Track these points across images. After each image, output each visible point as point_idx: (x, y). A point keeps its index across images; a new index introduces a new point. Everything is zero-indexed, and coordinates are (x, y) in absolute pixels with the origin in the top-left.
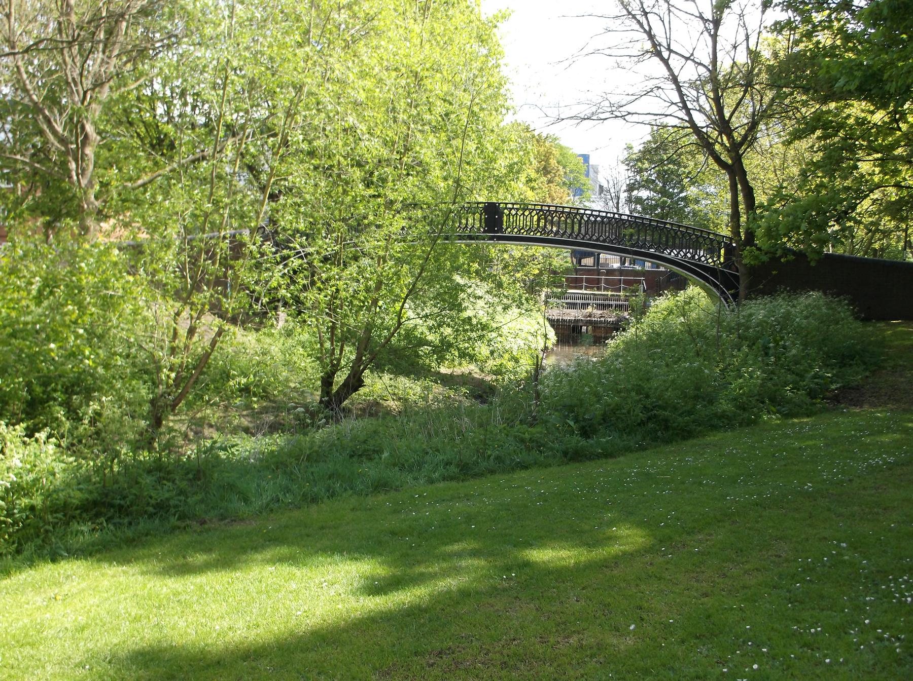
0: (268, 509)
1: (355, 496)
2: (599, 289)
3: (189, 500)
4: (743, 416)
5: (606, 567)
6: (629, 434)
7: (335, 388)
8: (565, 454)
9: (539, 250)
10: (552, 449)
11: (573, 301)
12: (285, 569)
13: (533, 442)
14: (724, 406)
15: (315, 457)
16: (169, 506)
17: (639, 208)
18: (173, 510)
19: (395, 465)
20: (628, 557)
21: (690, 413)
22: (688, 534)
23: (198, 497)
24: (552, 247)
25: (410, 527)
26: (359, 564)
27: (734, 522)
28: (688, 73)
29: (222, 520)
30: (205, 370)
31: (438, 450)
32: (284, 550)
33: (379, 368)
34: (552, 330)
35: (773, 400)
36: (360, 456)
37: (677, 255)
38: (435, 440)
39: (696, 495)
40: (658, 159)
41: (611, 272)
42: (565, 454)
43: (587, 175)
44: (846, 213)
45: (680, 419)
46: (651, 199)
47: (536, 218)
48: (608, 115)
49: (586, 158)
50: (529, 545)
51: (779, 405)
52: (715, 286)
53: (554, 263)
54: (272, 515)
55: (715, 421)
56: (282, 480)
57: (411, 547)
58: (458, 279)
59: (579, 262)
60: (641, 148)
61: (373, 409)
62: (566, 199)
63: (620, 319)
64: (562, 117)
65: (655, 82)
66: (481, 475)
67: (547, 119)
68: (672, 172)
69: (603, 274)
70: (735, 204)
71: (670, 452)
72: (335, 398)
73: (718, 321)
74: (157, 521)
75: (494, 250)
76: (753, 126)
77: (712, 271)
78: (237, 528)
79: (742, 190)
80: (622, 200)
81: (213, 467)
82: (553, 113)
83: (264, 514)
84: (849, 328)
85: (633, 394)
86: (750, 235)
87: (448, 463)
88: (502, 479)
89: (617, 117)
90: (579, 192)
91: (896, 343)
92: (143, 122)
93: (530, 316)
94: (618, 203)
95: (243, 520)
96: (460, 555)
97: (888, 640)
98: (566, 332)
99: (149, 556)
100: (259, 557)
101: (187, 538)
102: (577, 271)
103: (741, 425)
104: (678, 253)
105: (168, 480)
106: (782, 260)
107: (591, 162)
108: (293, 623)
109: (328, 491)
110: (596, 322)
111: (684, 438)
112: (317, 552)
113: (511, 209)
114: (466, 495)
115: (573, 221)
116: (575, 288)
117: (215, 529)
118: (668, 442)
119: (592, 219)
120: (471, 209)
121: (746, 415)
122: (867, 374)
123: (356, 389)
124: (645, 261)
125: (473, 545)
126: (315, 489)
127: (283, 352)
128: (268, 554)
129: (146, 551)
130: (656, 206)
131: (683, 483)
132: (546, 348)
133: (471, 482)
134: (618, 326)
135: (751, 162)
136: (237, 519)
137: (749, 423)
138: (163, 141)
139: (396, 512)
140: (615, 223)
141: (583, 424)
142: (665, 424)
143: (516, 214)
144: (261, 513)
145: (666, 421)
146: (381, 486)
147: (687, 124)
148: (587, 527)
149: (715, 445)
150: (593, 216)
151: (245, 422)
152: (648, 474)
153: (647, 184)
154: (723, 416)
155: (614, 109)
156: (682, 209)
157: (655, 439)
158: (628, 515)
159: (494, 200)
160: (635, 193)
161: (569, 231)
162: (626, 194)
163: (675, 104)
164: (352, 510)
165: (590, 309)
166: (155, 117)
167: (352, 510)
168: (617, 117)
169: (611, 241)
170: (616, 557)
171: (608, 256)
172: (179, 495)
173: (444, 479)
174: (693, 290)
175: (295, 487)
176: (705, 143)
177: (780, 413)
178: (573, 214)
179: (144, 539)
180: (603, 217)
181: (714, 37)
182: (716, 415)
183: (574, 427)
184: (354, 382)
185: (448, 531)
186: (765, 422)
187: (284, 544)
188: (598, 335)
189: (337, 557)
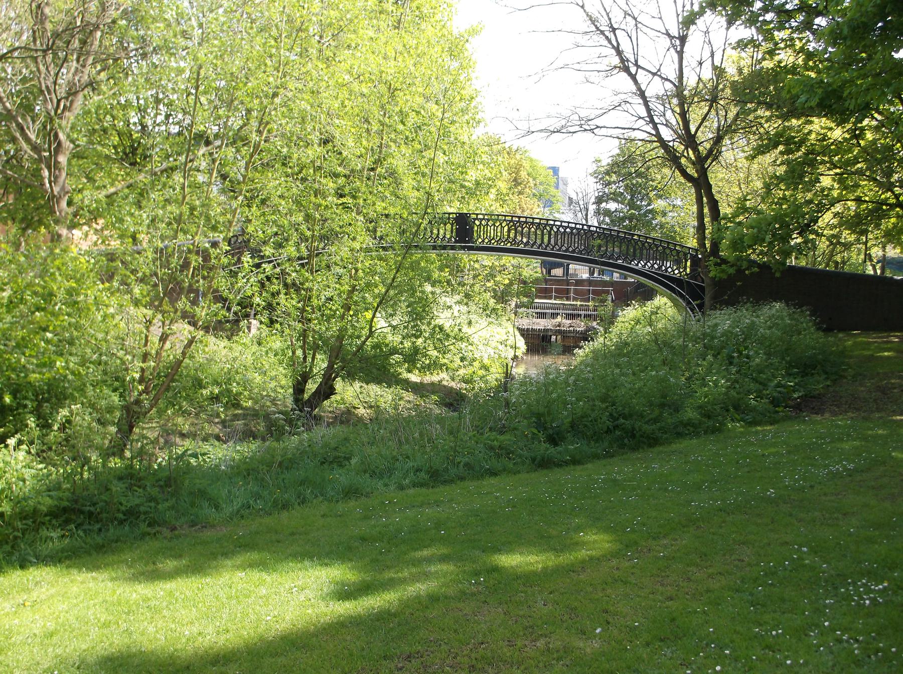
0: (238, 515)
2: (568, 299)
4: (709, 423)
7: (306, 396)
8: (534, 460)
9: (509, 260)
10: (520, 456)
12: (256, 575)
14: (690, 414)
15: (288, 464)
16: (140, 512)
18: (142, 517)
20: (594, 562)
21: (655, 421)
22: (654, 539)
23: (167, 504)
24: (522, 258)
28: (655, 88)
29: (193, 526)
31: (408, 457)
32: (255, 556)
33: (351, 376)
34: (522, 339)
35: (737, 408)
36: (331, 462)
40: (626, 172)
41: (580, 282)
42: (534, 460)
43: (557, 187)
44: (808, 225)
47: (506, 229)
48: (577, 128)
49: (555, 170)
50: (498, 550)
53: (524, 273)
55: (680, 429)
56: (252, 486)
57: (381, 553)
59: (549, 272)
60: (609, 161)
61: (347, 417)
62: (536, 210)
63: (589, 329)
64: (532, 129)
65: (623, 97)
66: (451, 481)
69: (572, 284)
70: (700, 216)
71: (638, 459)
72: (308, 401)
73: (684, 331)
74: (127, 528)
75: (465, 257)
76: (718, 140)
77: (678, 282)
78: (208, 534)
82: (524, 126)
83: (235, 520)
84: (810, 337)
86: (715, 245)
87: (418, 470)
88: (471, 485)
89: (586, 130)
90: (549, 203)
91: (856, 353)
94: (587, 215)
95: (213, 526)
96: (429, 560)
97: (847, 641)
98: (536, 342)
100: (229, 563)
101: (156, 544)
102: (546, 281)
105: (139, 487)
106: (747, 272)
107: (561, 174)
108: (262, 628)
109: (299, 497)
111: (651, 446)
112: (287, 558)
114: (436, 502)
115: (543, 232)
116: (545, 298)
118: (635, 449)
119: (562, 230)
120: (443, 220)
121: (711, 423)
122: (828, 383)
123: (327, 396)
125: (444, 551)
127: (256, 360)
128: (239, 560)
129: (115, 558)
131: (649, 489)
134: (586, 336)
135: (717, 176)
137: (714, 431)
138: (136, 149)
139: (366, 518)
140: (584, 234)
141: (551, 432)
143: (487, 225)
144: (231, 519)
146: (351, 492)
148: (554, 533)
149: (681, 453)
152: (615, 481)
153: (615, 197)
154: (689, 424)
155: (583, 122)
157: (622, 446)
158: (596, 520)
160: (604, 205)
161: (539, 242)
162: (594, 206)
163: (642, 118)
164: (323, 516)
165: (559, 319)
167: (323, 516)
168: (586, 130)
169: (580, 252)
170: (583, 561)
172: (150, 501)
174: (662, 301)
176: (673, 158)
177: (744, 421)
178: (543, 225)
179: (114, 545)
180: (572, 229)
181: (680, 54)
184: (326, 390)
185: (417, 537)
186: (729, 430)
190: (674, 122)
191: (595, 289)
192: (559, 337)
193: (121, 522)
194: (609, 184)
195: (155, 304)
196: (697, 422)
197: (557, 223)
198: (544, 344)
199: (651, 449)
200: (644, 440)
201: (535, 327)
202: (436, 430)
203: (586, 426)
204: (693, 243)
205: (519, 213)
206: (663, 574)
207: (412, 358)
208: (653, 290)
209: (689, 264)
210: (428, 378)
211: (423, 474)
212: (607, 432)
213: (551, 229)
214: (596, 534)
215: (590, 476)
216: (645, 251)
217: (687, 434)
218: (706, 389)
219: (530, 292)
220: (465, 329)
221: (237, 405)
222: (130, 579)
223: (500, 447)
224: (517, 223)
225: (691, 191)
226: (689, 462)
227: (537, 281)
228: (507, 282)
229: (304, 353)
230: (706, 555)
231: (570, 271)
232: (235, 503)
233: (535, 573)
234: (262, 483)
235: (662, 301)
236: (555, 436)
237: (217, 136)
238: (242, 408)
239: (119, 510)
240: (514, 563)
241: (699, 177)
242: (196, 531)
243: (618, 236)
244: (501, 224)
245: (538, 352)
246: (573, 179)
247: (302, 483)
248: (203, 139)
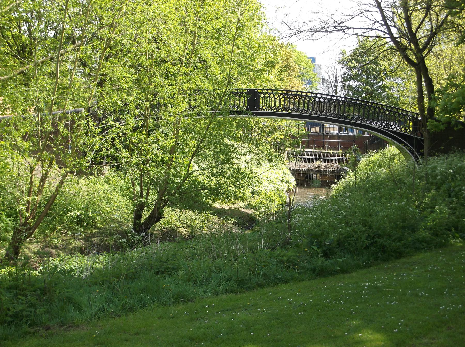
0: (96, 317)
1: (161, 306)
2: (324, 148)
3: (38, 311)
7: (143, 220)
8: (314, 270)
9: (284, 122)
10: (303, 268)
11: (307, 157)
16: (23, 316)
17: (350, 93)
18: (25, 319)
19: (189, 281)
21: (400, 239)
22: (417, 338)
23: (43, 309)
24: (292, 120)
27: (449, 328)
29: (62, 326)
30: (52, 206)
31: (220, 269)
33: (173, 205)
34: (293, 177)
36: (163, 273)
37: (375, 125)
39: (416, 305)
40: (363, 62)
41: (332, 137)
42: (314, 270)
43: (314, 71)
45: (394, 244)
46: (359, 87)
47: (283, 99)
48: (332, 29)
49: (313, 59)
51: (461, 232)
52: (405, 145)
53: (294, 131)
54: (100, 322)
56: (107, 294)
58: (227, 141)
59: (309, 130)
60: (351, 53)
61: (171, 235)
62: (301, 87)
64: (301, 29)
65: (363, 7)
67: (291, 32)
72: (143, 225)
73: (411, 172)
74: (13, 328)
75: (253, 121)
77: (404, 136)
78: (73, 333)
80: (339, 88)
81: (56, 284)
82: (295, 27)
83: (93, 321)
85: (361, 226)
87: (229, 280)
88: (269, 291)
89: (338, 30)
90: (309, 82)
93: (278, 167)
94: (336, 90)
95: (77, 326)
102: (309, 136)
103: (435, 248)
104: (376, 123)
105: (23, 295)
106: (455, 129)
107: (317, 62)
109: (141, 302)
111: (398, 258)
114: (244, 306)
115: (304, 101)
116: (308, 148)
118: (386, 260)
119: (322, 100)
120: (238, 93)
121: (438, 240)
123: (158, 220)
126: (131, 301)
127: (107, 194)
130: (363, 92)
132: (289, 189)
134: (338, 175)
135: (431, 62)
136: (73, 326)
137: (442, 246)
138: (25, 48)
139: (192, 320)
140: (334, 103)
141: (325, 248)
142: (383, 248)
144: (91, 320)
146: (180, 298)
147: (387, 36)
148: (339, 334)
150: (318, 97)
152: (376, 287)
153: (356, 77)
154: (422, 241)
155: (337, 25)
156: (379, 94)
157: (376, 259)
159: (253, 87)
160: (348, 83)
163: (378, 22)
164: (159, 318)
165: (318, 163)
166: (20, 32)
167: (159, 318)
168: (338, 30)
169: (336, 116)
171: (329, 126)
172: (31, 307)
173: (226, 292)
175: (116, 299)
176: (402, 49)
177: (462, 238)
180: (324, 99)
182: (418, 239)
183: (319, 251)
184: (157, 216)
186: (452, 245)
188: (324, 180)
190: (399, 23)
191: (345, 143)
192: (318, 175)
193: (10, 323)
197: (319, 96)
199: (398, 261)
200: (393, 254)
201: (302, 168)
202: (238, 248)
203: (349, 244)
204: (416, 109)
205: (289, 89)
207: (215, 193)
208: (384, 141)
209: (411, 124)
211: (232, 282)
212: (365, 248)
213: (310, 99)
214: (371, 334)
215: (357, 283)
216: (376, 115)
217: (422, 249)
218: (434, 215)
219: (300, 143)
223: (288, 261)
224: (289, 95)
225: (412, 72)
226: (428, 271)
227: (303, 135)
228: (282, 137)
229: (141, 189)
231: (325, 129)
232: (93, 308)
234: (113, 290)
236: (328, 251)
237: (80, 38)
239: (7, 315)
242: (65, 330)
243: (352, 103)
244: (279, 96)
245: (304, 185)
246: (325, 64)
247: (143, 291)
248: (71, 39)
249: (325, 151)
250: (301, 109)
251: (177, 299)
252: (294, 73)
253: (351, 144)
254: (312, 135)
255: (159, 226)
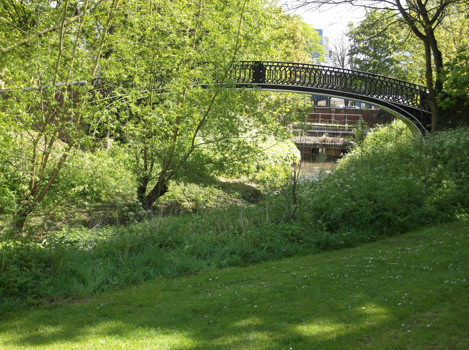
0: (100, 289)
1: (165, 279)
2: (330, 122)
5: (361, 341)
6: (363, 229)
7: (147, 193)
8: (318, 245)
9: (290, 95)
10: (308, 241)
13: (294, 236)
14: (429, 208)
15: (137, 249)
17: (358, 66)
19: (193, 254)
22: (420, 312)
23: (47, 282)
24: (298, 93)
25: (208, 306)
26: (170, 337)
29: (66, 298)
31: (224, 242)
32: (112, 324)
36: (166, 246)
37: (382, 98)
38: (221, 234)
40: (371, 34)
41: (338, 110)
43: (321, 44)
46: (366, 60)
47: (289, 72)
49: (320, 32)
50: (300, 321)
52: (412, 119)
53: (300, 104)
54: (103, 294)
55: (423, 220)
56: (110, 267)
57: (209, 324)
59: (316, 103)
61: (174, 208)
63: (345, 145)
68: (381, 42)
71: (394, 242)
72: (149, 197)
73: (418, 147)
74: (18, 300)
75: (260, 94)
77: (411, 110)
78: (78, 305)
79: (433, 54)
86: (439, 84)
87: (233, 253)
88: (273, 264)
90: (316, 55)
92: (14, 6)
94: (343, 63)
95: (81, 298)
96: (248, 329)
98: (308, 153)
99: (11, 328)
100: (92, 330)
101: (39, 313)
102: (315, 110)
103: (441, 222)
107: (324, 35)
109: (145, 275)
110: (328, 146)
111: (403, 232)
112: (137, 327)
113: (271, 66)
114: (248, 279)
115: (310, 74)
117: (61, 306)
118: (390, 235)
119: (328, 73)
120: (244, 66)
121: (444, 215)
123: (162, 193)
124: (361, 102)
127: (110, 168)
129: (8, 324)
130: (370, 65)
131: (409, 269)
133: (250, 267)
134: (344, 149)
135: (440, 34)
138: (27, 19)
139: (196, 293)
140: (341, 76)
141: (329, 222)
143: (270, 69)
144: (95, 292)
145: (389, 220)
146: (184, 271)
147: (396, 7)
148: (342, 307)
149: (425, 238)
151: (84, 217)
152: (381, 262)
153: (364, 50)
154: (427, 216)
157: (381, 233)
158: (372, 296)
164: (163, 290)
165: (324, 137)
167: (163, 290)
169: (342, 89)
173: (230, 265)
174: (398, 124)
179: (7, 313)
180: (331, 72)
182: (423, 214)
184: (162, 189)
185: (237, 309)
187: (112, 320)
189: (152, 331)
191: (351, 116)
192: (324, 149)
194: (358, 41)
195: (39, 126)
196: (434, 214)
198: (314, 154)
205: (296, 61)
206: (432, 343)
207: (220, 166)
208: (391, 115)
209: (419, 97)
210: (232, 180)
211: (236, 256)
214: (375, 307)
215: (361, 257)
217: (428, 223)
220: (260, 144)
221: (98, 200)
222: (18, 343)
223: (292, 235)
225: (420, 45)
226: (433, 245)
227: (309, 110)
229: (145, 162)
230: (463, 326)
231: (332, 103)
232: (97, 280)
233: (330, 342)
234: (116, 263)
235: (398, 124)
238: (102, 202)
240: (314, 333)
241: (428, 35)
242: (68, 302)
244: (285, 69)
245: (310, 159)
249: (331, 125)
250: (307, 81)
251: (181, 272)
252: (301, 45)
253: (358, 118)
254: (318, 109)
255: (163, 199)
